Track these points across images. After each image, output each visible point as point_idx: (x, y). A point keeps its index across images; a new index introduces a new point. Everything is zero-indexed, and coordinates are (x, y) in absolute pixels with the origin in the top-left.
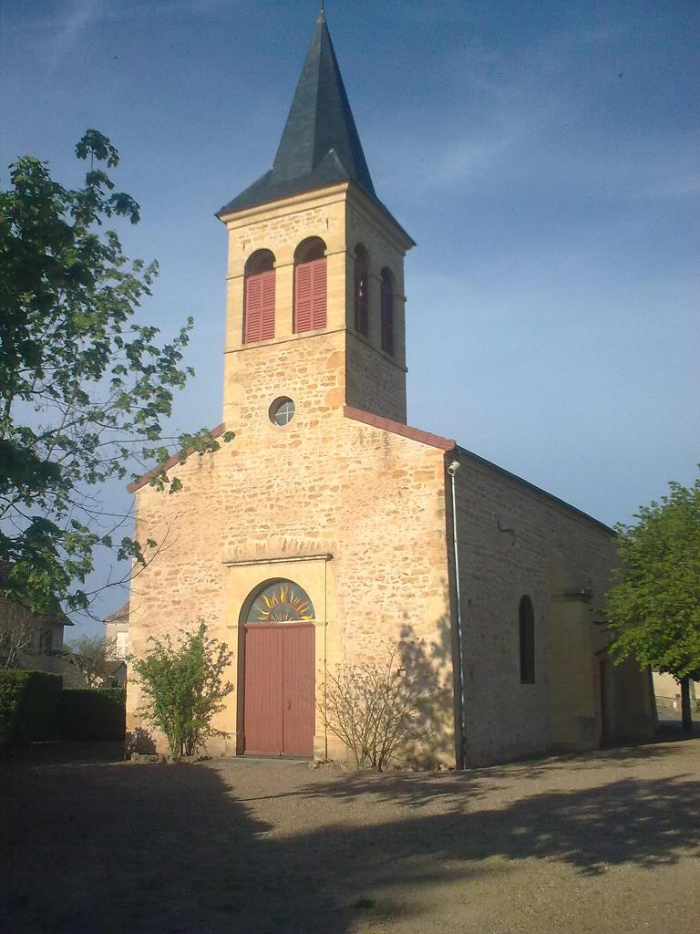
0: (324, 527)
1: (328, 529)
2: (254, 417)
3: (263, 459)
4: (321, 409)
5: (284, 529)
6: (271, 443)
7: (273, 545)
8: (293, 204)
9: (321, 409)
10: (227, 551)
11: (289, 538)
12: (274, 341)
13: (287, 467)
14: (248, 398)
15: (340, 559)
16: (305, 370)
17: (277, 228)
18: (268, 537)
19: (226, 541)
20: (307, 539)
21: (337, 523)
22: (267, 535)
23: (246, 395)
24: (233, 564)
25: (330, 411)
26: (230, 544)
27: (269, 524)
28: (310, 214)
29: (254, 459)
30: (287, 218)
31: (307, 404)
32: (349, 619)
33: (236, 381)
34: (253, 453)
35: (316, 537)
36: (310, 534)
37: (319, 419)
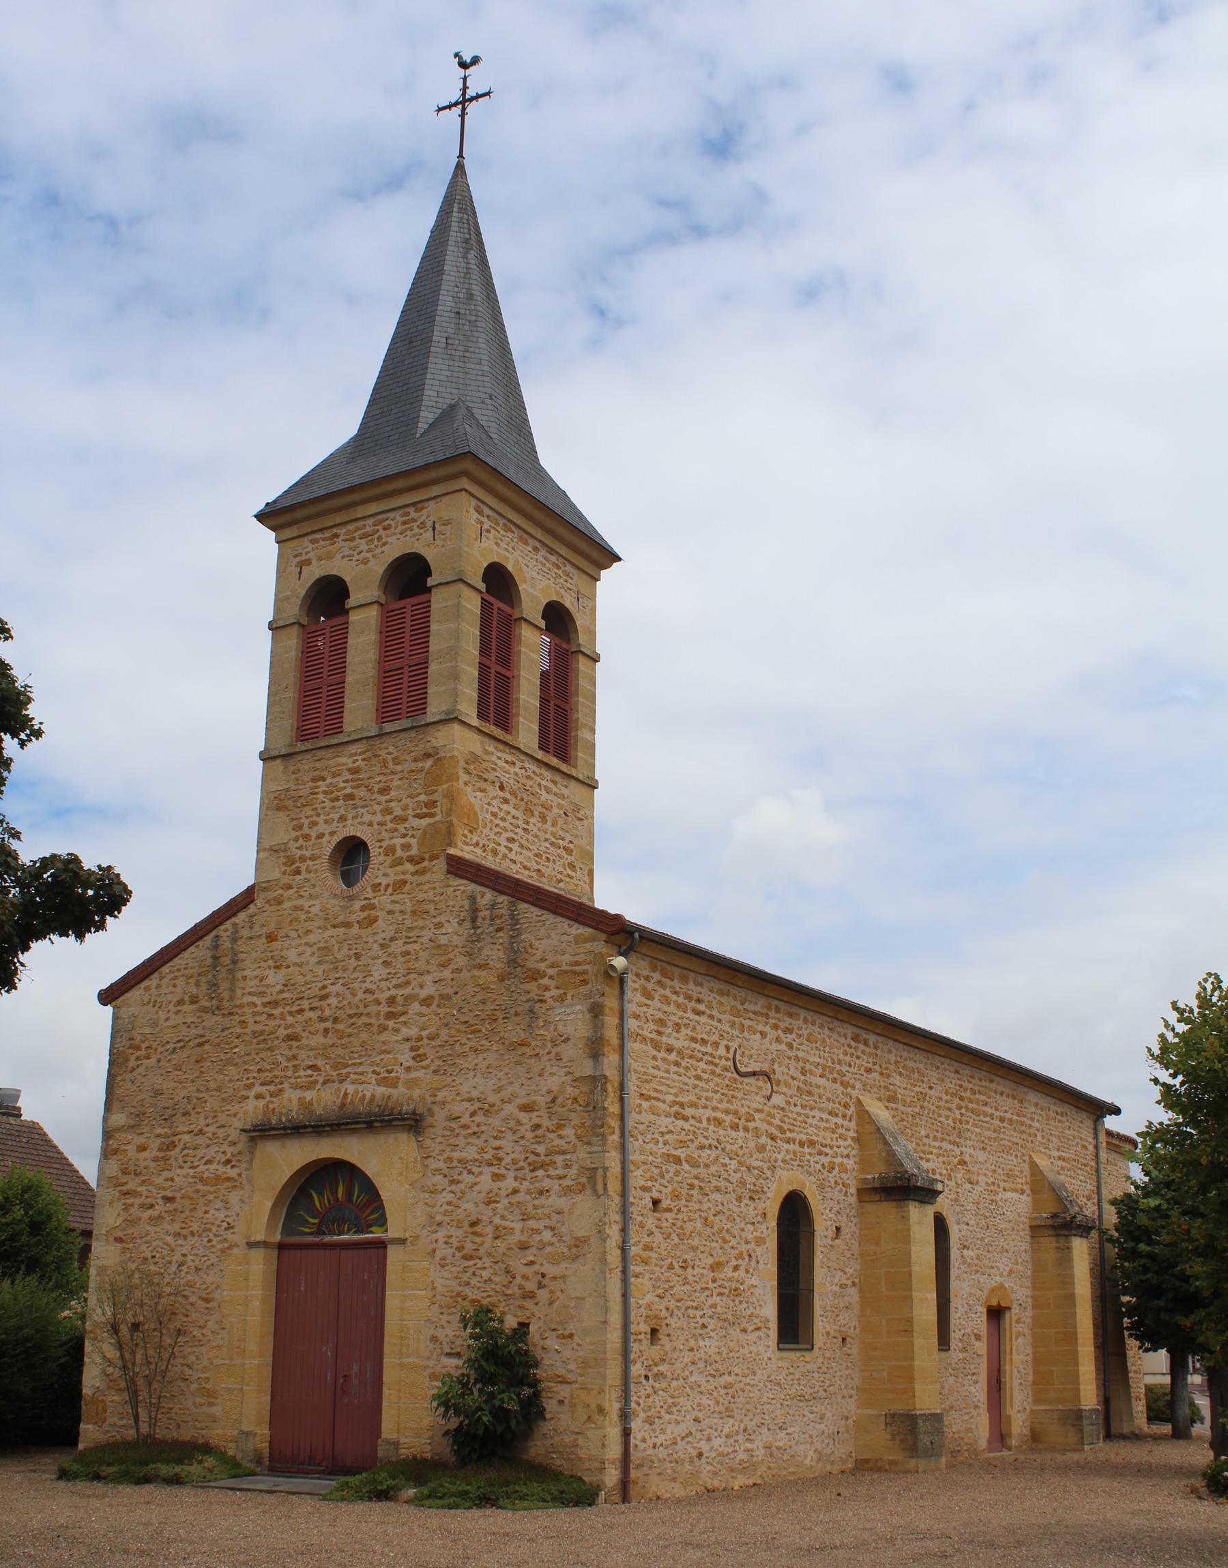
0: (408, 1069)
1: (414, 1074)
5: (344, 1071)
7: (325, 1099)
10: (252, 1110)
11: (351, 1089)
14: (296, 840)
18: (319, 1086)
19: (252, 1093)
20: (381, 1090)
21: (428, 1062)
22: (316, 1082)
24: (261, 1132)
25: (426, 863)
26: (259, 1097)
27: (320, 1063)
30: (370, 521)
31: (390, 851)
32: (441, 1236)
33: (279, 809)
35: (395, 1086)
36: (383, 1082)
37: (408, 877)
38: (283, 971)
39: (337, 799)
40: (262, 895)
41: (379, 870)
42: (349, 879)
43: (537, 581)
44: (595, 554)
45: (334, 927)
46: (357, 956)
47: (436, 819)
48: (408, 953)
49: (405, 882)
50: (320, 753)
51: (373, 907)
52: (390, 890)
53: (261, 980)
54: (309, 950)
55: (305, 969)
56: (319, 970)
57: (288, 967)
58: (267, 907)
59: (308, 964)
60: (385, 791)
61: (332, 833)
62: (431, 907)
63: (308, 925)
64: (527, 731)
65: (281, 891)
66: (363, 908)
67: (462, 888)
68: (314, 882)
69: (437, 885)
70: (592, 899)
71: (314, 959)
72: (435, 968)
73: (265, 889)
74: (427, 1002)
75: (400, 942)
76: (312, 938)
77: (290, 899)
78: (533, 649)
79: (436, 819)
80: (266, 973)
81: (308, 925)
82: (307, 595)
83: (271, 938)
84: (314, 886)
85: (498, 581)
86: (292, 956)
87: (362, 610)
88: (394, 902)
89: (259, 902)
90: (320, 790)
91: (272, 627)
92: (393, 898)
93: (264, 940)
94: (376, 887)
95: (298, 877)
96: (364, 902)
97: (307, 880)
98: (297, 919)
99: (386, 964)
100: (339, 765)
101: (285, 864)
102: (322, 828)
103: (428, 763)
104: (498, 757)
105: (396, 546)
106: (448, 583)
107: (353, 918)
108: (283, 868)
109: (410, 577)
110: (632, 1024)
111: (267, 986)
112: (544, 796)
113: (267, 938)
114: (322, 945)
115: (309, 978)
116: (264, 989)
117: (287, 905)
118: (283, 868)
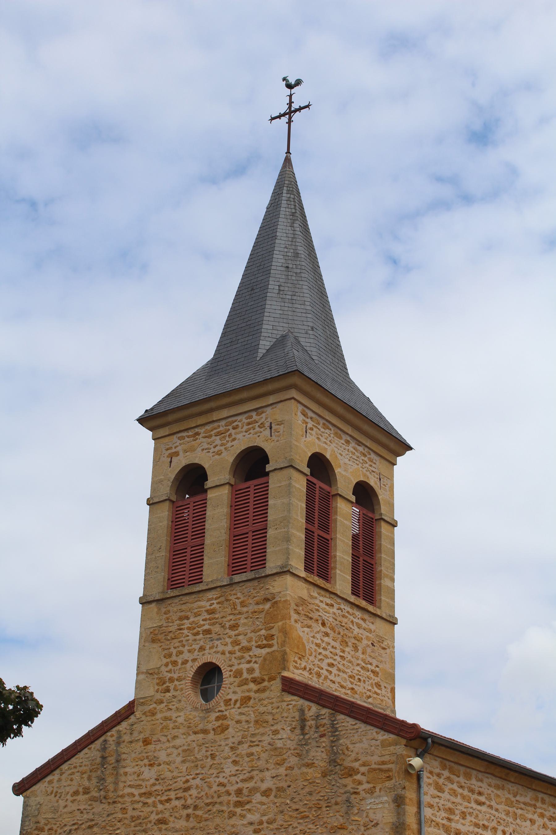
14: (167, 665)
29: (169, 751)
31: (238, 673)
33: (153, 641)
34: (168, 741)
37: (252, 694)
38: (156, 768)
39: (197, 634)
41: (230, 689)
42: (207, 695)
43: (349, 466)
44: (392, 445)
45: (195, 733)
46: (213, 756)
47: (273, 649)
48: (252, 754)
49: (249, 698)
52: (238, 705)
53: (138, 776)
54: (176, 752)
56: (184, 768)
57: (159, 765)
60: (234, 627)
61: (194, 660)
62: (269, 718)
64: (343, 580)
65: (155, 705)
67: (293, 703)
68: (180, 698)
69: (274, 700)
71: (179, 759)
72: (273, 766)
73: (143, 704)
74: (266, 793)
75: (245, 746)
76: (178, 742)
78: (346, 518)
79: (273, 649)
83: (146, 742)
84: (180, 701)
85: (320, 466)
86: (163, 756)
88: (241, 714)
90: (186, 626)
92: (240, 710)
93: (141, 743)
95: (168, 694)
96: (218, 714)
98: (166, 727)
99: (235, 762)
101: (158, 684)
102: (186, 656)
103: (267, 606)
104: (320, 601)
105: (242, 441)
106: (281, 468)
108: (157, 687)
109: (253, 465)
110: (427, 812)
111: (143, 780)
112: (356, 630)
113: (143, 742)
116: (140, 783)
117: (159, 716)
118: (157, 687)
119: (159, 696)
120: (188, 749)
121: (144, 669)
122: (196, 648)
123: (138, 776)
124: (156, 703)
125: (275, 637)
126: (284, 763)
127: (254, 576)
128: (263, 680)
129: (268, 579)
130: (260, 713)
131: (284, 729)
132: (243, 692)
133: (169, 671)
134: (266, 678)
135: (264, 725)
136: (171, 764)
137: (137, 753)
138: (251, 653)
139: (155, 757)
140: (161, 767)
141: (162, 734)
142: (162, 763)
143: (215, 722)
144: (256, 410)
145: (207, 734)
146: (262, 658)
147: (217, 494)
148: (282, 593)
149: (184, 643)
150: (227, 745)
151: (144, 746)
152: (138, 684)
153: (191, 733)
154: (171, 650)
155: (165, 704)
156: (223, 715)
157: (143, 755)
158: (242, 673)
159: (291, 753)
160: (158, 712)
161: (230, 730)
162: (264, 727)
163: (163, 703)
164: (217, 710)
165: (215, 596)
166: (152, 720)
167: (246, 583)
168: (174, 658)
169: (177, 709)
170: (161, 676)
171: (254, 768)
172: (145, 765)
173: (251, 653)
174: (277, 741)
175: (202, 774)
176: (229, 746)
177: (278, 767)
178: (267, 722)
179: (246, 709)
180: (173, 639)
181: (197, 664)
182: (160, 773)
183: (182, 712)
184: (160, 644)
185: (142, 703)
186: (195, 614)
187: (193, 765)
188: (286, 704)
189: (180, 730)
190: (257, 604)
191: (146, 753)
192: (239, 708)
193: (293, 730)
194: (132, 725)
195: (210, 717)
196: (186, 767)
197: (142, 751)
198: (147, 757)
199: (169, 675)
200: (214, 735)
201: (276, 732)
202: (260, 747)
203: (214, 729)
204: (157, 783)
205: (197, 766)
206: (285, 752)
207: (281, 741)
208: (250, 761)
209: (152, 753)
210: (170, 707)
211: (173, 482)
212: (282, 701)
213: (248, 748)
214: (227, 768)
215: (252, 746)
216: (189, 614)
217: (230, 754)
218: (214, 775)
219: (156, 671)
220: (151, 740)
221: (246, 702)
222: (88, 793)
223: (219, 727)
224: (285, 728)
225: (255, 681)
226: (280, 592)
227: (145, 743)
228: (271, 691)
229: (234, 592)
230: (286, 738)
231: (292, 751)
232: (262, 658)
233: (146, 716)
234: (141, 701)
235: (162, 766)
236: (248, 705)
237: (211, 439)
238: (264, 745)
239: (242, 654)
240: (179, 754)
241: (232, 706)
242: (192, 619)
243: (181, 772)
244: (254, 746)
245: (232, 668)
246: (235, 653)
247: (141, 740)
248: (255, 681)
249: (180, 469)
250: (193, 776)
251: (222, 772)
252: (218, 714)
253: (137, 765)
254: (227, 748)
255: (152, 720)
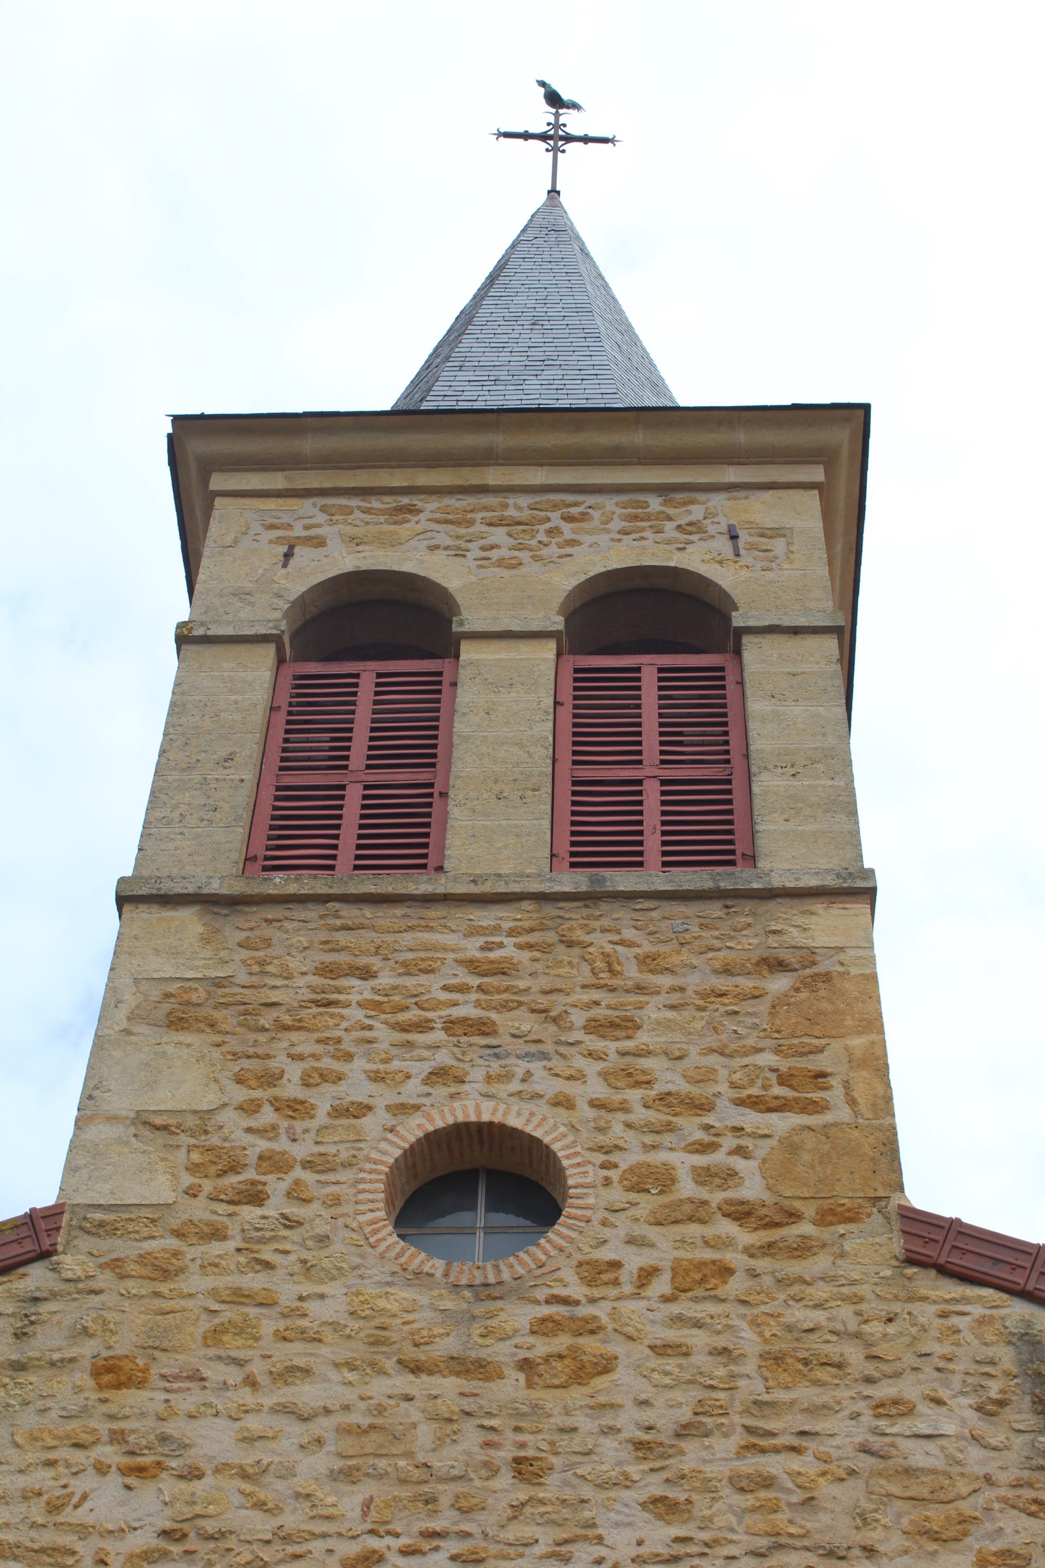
2: (275, 1206)
3: (323, 1426)
4: (741, 1213)
6: (378, 1344)
8: (919, 1253)
9: (741, 1213)
12: (741, 877)
13: (506, 1488)
14: (250, 1108)
15: (842, 1355)
16: (621, 1026)
17: (471, 523)
23: (240, 1094)
25: (805, 1228)
28: (645, 505)
29: (254, 1423)
30: (524, 500)
31: (649, 1180)
33: (176, 1022)
34: (251, 1382)
37: (733, 1258)
38: (168, 1486)
39: (423, 1026)
40: (85, 1243)
45: (416, 1369)
46: (526, 1469)
47: (828, 1117)
48: (767, 1482)
49: (726, 1272)
50: (350, 913)
51: (591, 1328)
52: (662, 1285)
53: (54, 1508)
54: (294, 1431)
55: (274, 1489)
56: (348, 1502)
57: (194, 1474)
58: (104, 1279)
59: (288, 1473)
60: (621, 1026)
61: (402, 1109)
62: (854, 1355)
63: (295, 1353)
65: (172, 1243)
66: (543, 1327)
67: (977, 1311)
68: (323, 1229)
69: (865, 1290)
70: (657, 384)
71: (321, 1462)
72: (897, 1541)
73: (101, 1229)
75: (724, 1446)
76: (306, 1394)
77: (209, 1266)
79: (828, 1117)
80: (79, 1486)
81: (295, 1353)
82: (302, 602)
83: (113, 1374)
84: (323, 1240)
86: (214, 1440)
87: (504, 644)
88: (678, 1320)
89: (71, 1263)
90: (354, 998)
91: (126, 899)
92: (675, 1309)
93: (82, 1377)
94: (599, 1273)
95: (249, 1213)
96: (546, 1310)
97: (290, 1223)
98: (244, 1329)
99: (662, 1507)
100: (434, 948)
101: (193, 1168)
102: (356, 1087)
103: (779, 984)
106: (796, 631)
107: (501, 1352)
108: (187, 1180)
111: (83, 1531)
113: (96, 1373)
114: (356, 1418)
115: (293, 1519)
116: (67, 1540)
117: (196, 1282)
118: (187, 1180)
119: (200, 1210)
120: (373, 1427)
121: (122, 1102)
122: (414, 1071)
123: (54, 1508)
124: (178, 1234)
125: (833, 1081)
126: (965, 1534)
127: (709, 884)
128: (794, 1216)
129: (772, 905)
130: (789, 1328)
131: (939, 1402)
132: (682, 1242)
133: (269, 1132)
134: (809, 1210)
135: (822, 1374)
136: (267, 1479)
137: (53, 1414)
138: (710, 1119)
139: (164, 1439)
140: (198, 1487)
141: (212, 1352)
142: (207, 1468)
143: (531, 1340)
144: (663, 490)
145: (487, 1379)
146: (773, 1142)
147: (503, 655)
148: (851, 952)
149: (347, 1046)
150: (610, 1431)
151: (101, 1388)
152: (79, 1150)
153: (390, 1364)
154: (273, 1064)
155: (231, 1245)
156: (572, 1318)
157: (93, 1424)
158: (674, 1181)
159: (1004, 1500)
160: (194, 1268)
161: (621, 1374)
162: (818, 1383)
163: (225, 1238)
164: (541, 1294)
165: (506, 925)
166: (157, 1294)
167: (665, 904)
168: (291, 1089)
169: (307, 1268)
170: (215, 1140)
171: (783, 1540)
172: (102, 1470)
173: (710, 1119)
174: (907, 1445)
175: (467, 1535)
176: (625, 1435)
177: (932, 1546)
178: (839, 1366)
179: (712, 1308)
180: (287, 1028)
181: (414, 1129)
182: (198, 1509)
183: (337, 1284)
184: (218, 1038)
185: (102, 1224)
186: (404, 964)
187: (406, 1493)
188: (931, 1309)
189: (324, 1350)
190: (727, 971)
191: (112, 1417)
192: (666, 1299)
193: (990, 1409)
194: (36, 1300)
195: (503, 1316)
196: (359, 1499)
197: (85, 1409)
198: (117, 1437)
199: (263, 1145)
200: (530, 1385)
201: (896, 1408)
202: (809, 1458)
203: (526, 1365)
204: (176, 1549)
205: (430, 1500)
206: (964, 1490)
207: (931, 1446)
208: (753, 1510)
209: (150, 1422)
210: (267, 1255)
211: (293, 604)
212: (910, 1299)
213: (739, 1456)
214: (617, 1525)
215: (763, 1451)
216: (376, 963)
217: (634, 1470)
218: (538, 1550)
219: (191, 1121)
220: (146, 1370)
221: (703, 1280)
222: (186, 1552)
223: (561, 1357)
224: (944, 1394)
225: (748, 1214)
226: (842, 949)
227: (107, 1378)
228: (842, 1255)
229: (605, 922)
230: (959, 1437)
231: (1003, 1492)
232: (773, 1142)
233: (122, 1277)
234: (98, 1216)
235: (209, 1480)
236: (720, 1292)
237: (471, 530)
238: (835, 1453)
239: (664, 1117)
240: (319, 1441)
241: (628, 1289)
242: (385, 980)
243: (328, 1518)
244: (776, 1450)
245: (613, 1158)
246: (627, 1111)
247: (87, 1363)
248: (748, 1214)
249: (321, 578)
250: (403, 1541)
251: (585, 1538)
252: (546, 1310)
253: (50, 1464)
254: (609, 1443)
255: (157, 1294)
